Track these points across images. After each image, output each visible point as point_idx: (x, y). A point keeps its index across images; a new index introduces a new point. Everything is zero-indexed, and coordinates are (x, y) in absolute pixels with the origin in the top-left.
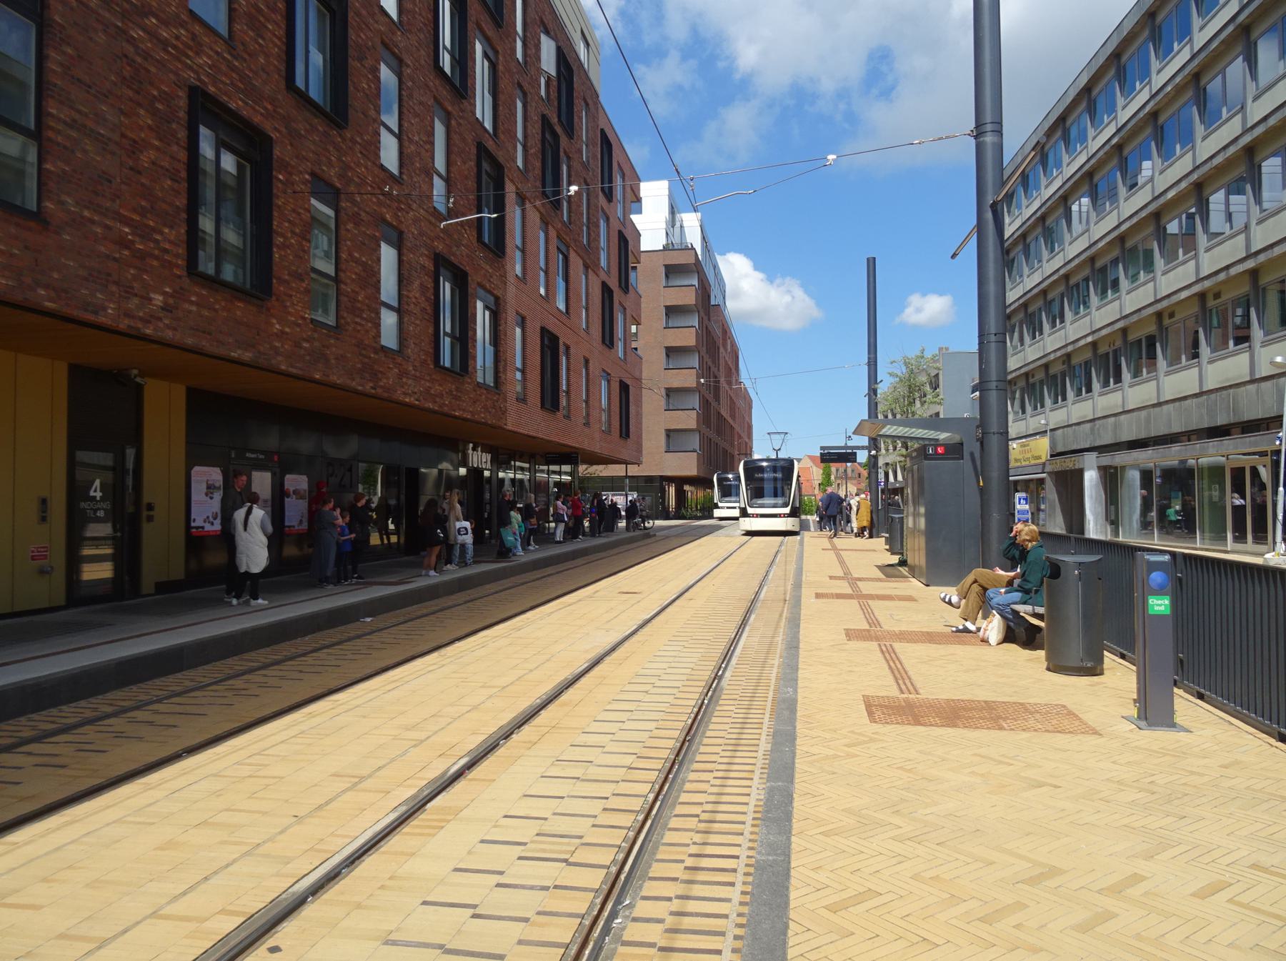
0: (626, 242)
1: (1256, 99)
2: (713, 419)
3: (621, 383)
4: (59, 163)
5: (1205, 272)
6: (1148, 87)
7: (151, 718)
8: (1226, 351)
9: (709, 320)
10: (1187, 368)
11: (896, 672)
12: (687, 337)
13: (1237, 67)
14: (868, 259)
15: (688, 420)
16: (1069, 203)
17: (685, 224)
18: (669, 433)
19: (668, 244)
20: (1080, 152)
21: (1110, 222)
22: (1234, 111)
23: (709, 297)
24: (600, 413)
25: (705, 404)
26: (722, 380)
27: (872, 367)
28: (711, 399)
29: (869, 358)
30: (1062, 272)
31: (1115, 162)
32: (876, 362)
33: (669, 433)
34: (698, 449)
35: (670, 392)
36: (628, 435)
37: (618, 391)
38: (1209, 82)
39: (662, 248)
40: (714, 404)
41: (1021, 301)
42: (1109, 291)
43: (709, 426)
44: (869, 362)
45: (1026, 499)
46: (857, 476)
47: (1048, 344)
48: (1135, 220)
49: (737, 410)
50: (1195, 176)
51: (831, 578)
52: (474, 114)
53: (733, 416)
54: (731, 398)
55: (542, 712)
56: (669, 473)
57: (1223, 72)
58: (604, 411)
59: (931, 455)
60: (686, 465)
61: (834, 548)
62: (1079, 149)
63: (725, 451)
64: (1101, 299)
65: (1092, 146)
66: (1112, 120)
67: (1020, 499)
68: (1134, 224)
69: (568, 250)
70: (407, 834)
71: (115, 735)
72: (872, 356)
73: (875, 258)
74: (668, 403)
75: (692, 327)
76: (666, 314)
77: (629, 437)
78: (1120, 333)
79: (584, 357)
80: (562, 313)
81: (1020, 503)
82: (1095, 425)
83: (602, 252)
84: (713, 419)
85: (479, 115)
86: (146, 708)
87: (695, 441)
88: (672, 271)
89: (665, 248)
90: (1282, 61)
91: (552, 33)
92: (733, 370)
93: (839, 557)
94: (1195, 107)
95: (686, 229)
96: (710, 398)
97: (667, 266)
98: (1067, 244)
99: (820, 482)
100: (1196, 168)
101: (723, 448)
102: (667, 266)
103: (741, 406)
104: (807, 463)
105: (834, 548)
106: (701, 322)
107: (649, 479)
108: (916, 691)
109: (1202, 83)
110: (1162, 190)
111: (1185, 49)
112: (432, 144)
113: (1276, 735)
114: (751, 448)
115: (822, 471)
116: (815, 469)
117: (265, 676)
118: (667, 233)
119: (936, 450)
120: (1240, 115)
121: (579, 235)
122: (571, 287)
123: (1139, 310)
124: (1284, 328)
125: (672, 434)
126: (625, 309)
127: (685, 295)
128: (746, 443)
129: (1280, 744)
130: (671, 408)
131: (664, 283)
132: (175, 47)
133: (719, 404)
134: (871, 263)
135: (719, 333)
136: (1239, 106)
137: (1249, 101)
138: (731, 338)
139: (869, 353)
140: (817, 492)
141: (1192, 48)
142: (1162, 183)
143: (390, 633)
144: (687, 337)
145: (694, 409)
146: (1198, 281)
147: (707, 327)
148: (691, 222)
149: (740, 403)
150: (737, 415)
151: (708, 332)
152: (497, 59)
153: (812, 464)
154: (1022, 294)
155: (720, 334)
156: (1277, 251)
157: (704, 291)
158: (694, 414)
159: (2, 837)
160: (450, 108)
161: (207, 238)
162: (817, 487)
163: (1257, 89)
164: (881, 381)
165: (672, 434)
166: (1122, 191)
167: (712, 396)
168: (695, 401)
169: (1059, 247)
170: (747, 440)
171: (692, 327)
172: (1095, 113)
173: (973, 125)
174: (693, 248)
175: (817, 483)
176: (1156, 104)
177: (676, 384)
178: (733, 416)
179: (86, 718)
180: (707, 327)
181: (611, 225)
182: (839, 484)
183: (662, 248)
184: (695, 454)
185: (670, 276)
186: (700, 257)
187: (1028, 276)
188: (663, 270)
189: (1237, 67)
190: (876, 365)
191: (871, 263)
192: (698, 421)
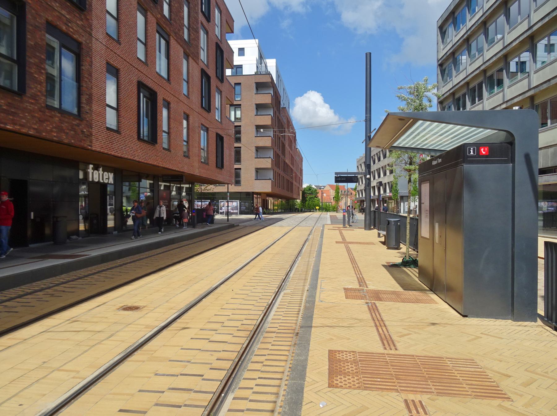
0: (222, 52)
1: (535, 11)
2: (281, 165)
3: (218, 135)
4: (33, 62)
5: (534, 84)
6: (465, 27)
7: (64, 289)
8: (546, 127)
9: (280, 114)
10: (551, 129)
11: (358, 270)
12: (266, 120)
13: (502, 19)
14: (366, 54)
15: (267, 163)
16: (509, 6)
17: (268, 65)
18: (257, 170)
19: (257, 72)
20: (478, 11)
21: (450, 86)
22: (523, 19)
23: (280, 102)
24: (199, 151)
25: (277, 156)
26: (287, 146)
27: (368, 122)
28: (280, 153)
29: (366, 117)
30: (482, 68)
31: (451, 60)
32: (370, 119)
33: (257, 170)
34: (272, 178)
35: (258, 149)
36: (222, 167)
37: (215, 139)
38: (490, 26)
39: (254, 74)
40: (281, 156)
41: (451, 91)
42: (496, 87)
43: (279, 167)
44: (366, 119)
46: (350, 194)
47: (487, 105)
48: (547, 19)
49: (294, 161)
50: (504, 51)
51: (337, 242)
53: (293, 164)
54: (291, 155)
55: (203, 299)
56: (257, 191)
57: (496, 21)
58: (203, 150)
59: (472, 156)
60: (265, 186)
61: (344, 241)
62: (461, 27)
63: (288, 181)
64: (490, 94)
65: (454, 39)
66: (480, 9)
68: (544, 24)
69: (169, 37)
70: (169, 330)
71: (38, 299)
72: (368, 115)
73: (370, 53)
74: (257, 154)
75: (269, 115)
76: (256, 109)
77: (223, 168)
78: (528, 101)
79: (185, 113)
80: (164, 78)
83: (202, 51)
84: (281, 165)
86: (24, 297)
87: (271, 175)
88: (260, 86)
89: (256, 74)
90: (520, 16)
92: (293, 142)
93: (349, 251)
94: (467, 51)
95: (268, 67)
96: (280, 153)
97: (257, 83)
98: (454, 77)
99: (334, 196)
100: (484, 63)
101: (287, 180)
102: (257, 83)
103: (297, 159)
104: (328, 188)
105: (344, 241)
106: (275, 113)
107: (248, 194)
108: (366, 286)
109: (470, 42)
110: (535, 22)
111: (480, 11)
113: (554, 328)
114: (302, 180)
115: (335, 191)
116: (331, 190)
117: (106, 274)
118: (257, 67)
120: (527, 20)
121: (179, 30)
122: (172, 62)
123: (549, 80)
124: (555, 120)
125: (259, 171)
126: (221, 92)
127: (266, 98)
128: (299, 178)
129: (555, 332)
130: (259, 157)
131: (255, 92)
133: (285, 157)
134: (369, 56)
135: (285, 121)
136: (527, 16)
137: (532, 12)
138: (292, 125)
139: (366, 114)
140: (332, 201)
141: (483, 10)
142: (509, 38)
143: (155, 258)
144: (266, 120)
145: (270, 158)
146: (530, 90)
147: (278, 117)
148: (271, 64)
149: (297, 158)
150: (295, 164)
151: (279, 120)
153: (330, 189)
154: (452, 87)
155: (286, 122)
156: (553, 82)
157: (277, 98)
158: (270, 160)
159: (1, 337)
161: (56, 79)
162: (332, 199)
163: (536, 6)
164: (363, 143)
165: (259, 171)
166: (486, 46)
167: (281, 152)
168: (271, 154)
169: (449, 79)
170: (300, 176)
171: (269, 115)
172: (456, 24)
173: (365, 119)
175: (332, 197)
176: (485, 18)
177: (261, 144)
178: (293, 164)
179: (20, 295)
180: (278, 117)
181: (209, 37)
182: (342, 198)
183: (254, 74)
184: (271, 181)
185: (259, 89)
186: (275, 82)
187: (456, 77)
188: (255, 85)
189: (502, 19)
190: (371, 121)
191: (369, 56)
192: (272, 164)
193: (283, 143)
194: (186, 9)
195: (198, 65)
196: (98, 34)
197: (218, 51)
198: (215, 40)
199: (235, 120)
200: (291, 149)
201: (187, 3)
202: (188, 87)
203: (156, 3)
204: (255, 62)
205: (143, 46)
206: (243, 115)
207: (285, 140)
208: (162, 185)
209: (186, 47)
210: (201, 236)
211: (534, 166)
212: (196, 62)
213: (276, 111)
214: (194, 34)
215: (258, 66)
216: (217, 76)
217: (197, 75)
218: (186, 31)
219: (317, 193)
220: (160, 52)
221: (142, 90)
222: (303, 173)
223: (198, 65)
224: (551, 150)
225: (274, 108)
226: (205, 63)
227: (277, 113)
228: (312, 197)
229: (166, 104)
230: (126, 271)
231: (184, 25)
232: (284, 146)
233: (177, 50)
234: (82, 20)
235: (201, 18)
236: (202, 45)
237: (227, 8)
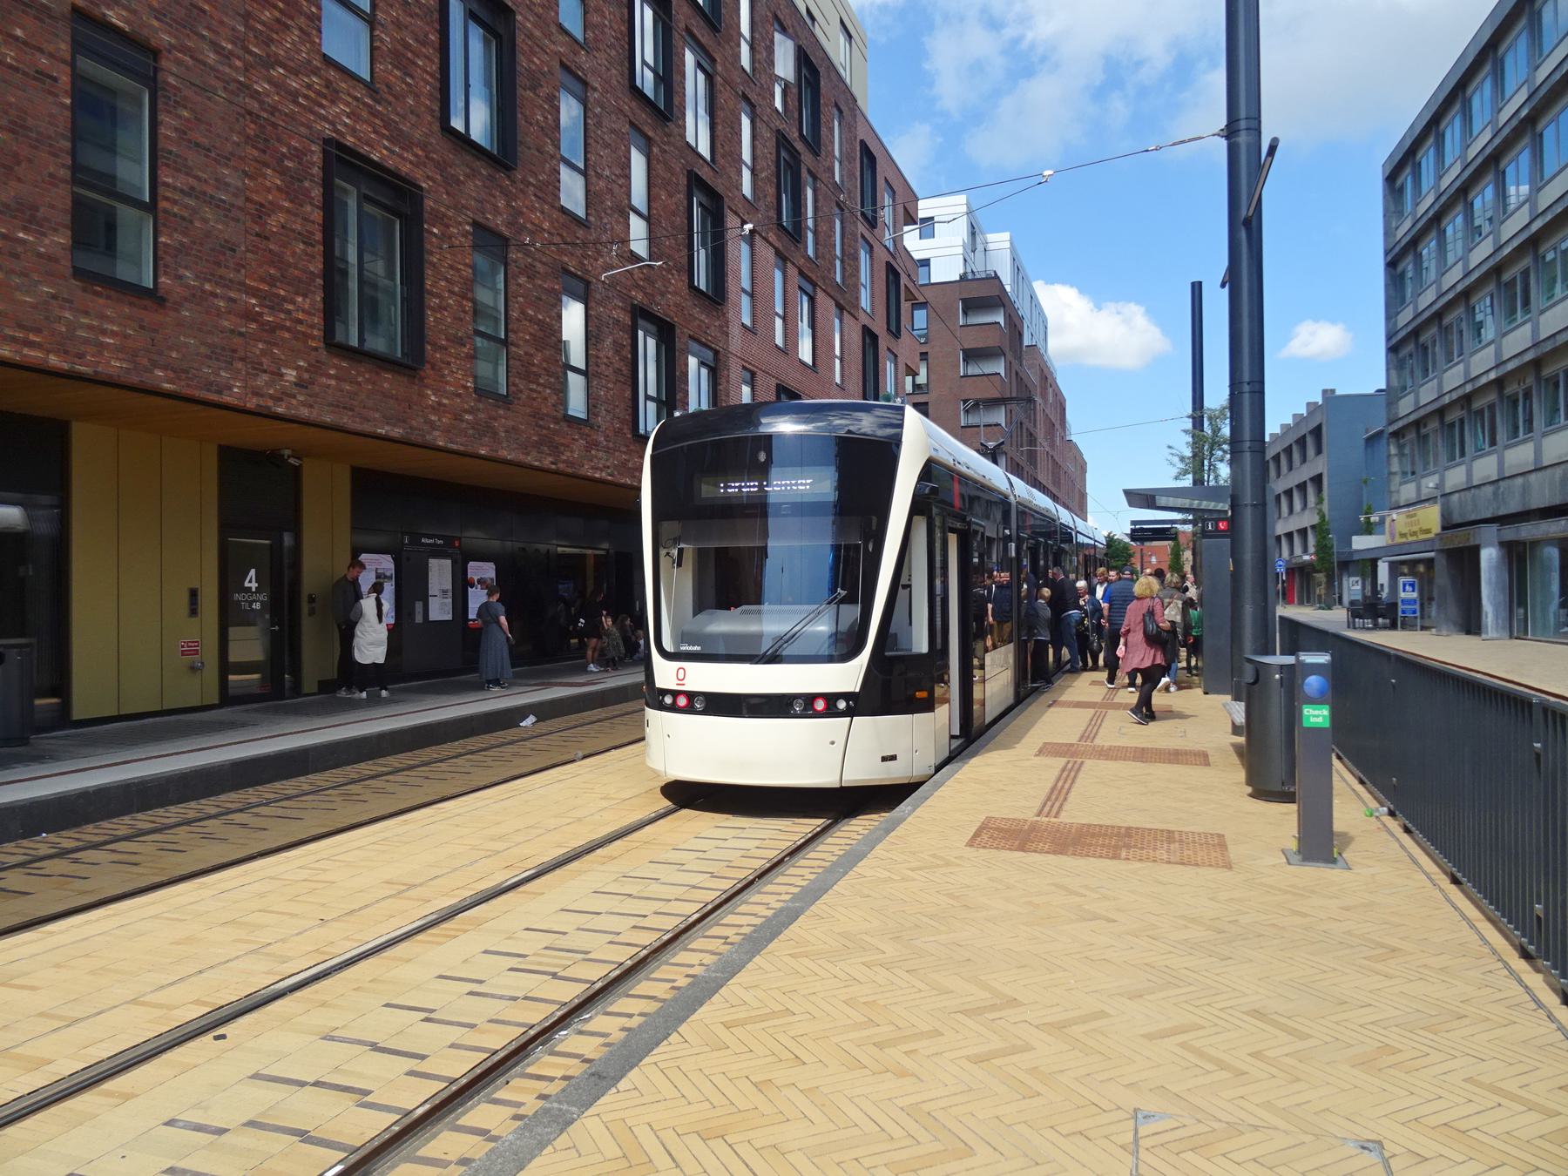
23: (1021, 335)
39: (958, 278)
45: (1412, 585)
49: (1062, 473)
52: (683, 136)
58: (647, 397)
59: (1210, 531)
67: (1404, 585)
69: (815, 291)
75: (997, 374)
81: (1404, 591)
82: (1498, 488)
85: (690, 138)
89: (963, 278)
91: (790, 30)
92: (1057, 426)
112: (628, 177)
119: (1217, 524)
122: (818, 334)
132: (306, 97)
133: (1036, 469)
135: (1034, 378)
147: (1017, 373)
149: (1071, 467)
152: (714, 67)
160: (650, 134)
174: (997, 277)
180: (1017, 373)
183: (958, 278)
185: (969, 313)
193: (1031, 434)
194: (746, 123)
195: (857, 319)
196: (735, 331)
197: (891, 277)
198: (886, 257)
199: (914, 390)
200: (1052, 445)
201: (748, 109)
202: (753, 307)
203: (798, 242)
204: (960, 250)
205: (749, 298)
206: (933, 377)
207: (1035, 426)
208: (1282, 559)
209: (838, 297)
210: (371, 756)
211: (1269, 532)
212: (854, 317)
213: (1013, 361)
214: (851, 266)
215: (968, 258)
216: (888, 329)
217: (856, 337)
218: (746, 175)
219: (1131, 556)
220: (802, 321)
221: (641, 322)
222: (1089, 510)
223: (857, 319)
224: (1558, 471)
225: (1007, 354)
226: (868, 311)
227: (1016, 366)
228: (225, 286)
229: (748, 375)
230: (295, 814)
231: (807, 227)
232: (1032, 440)
233: (825, 304)
234: (718, 318)
235: (862, 228)
236: (863, 280)
237: (905, 180)
